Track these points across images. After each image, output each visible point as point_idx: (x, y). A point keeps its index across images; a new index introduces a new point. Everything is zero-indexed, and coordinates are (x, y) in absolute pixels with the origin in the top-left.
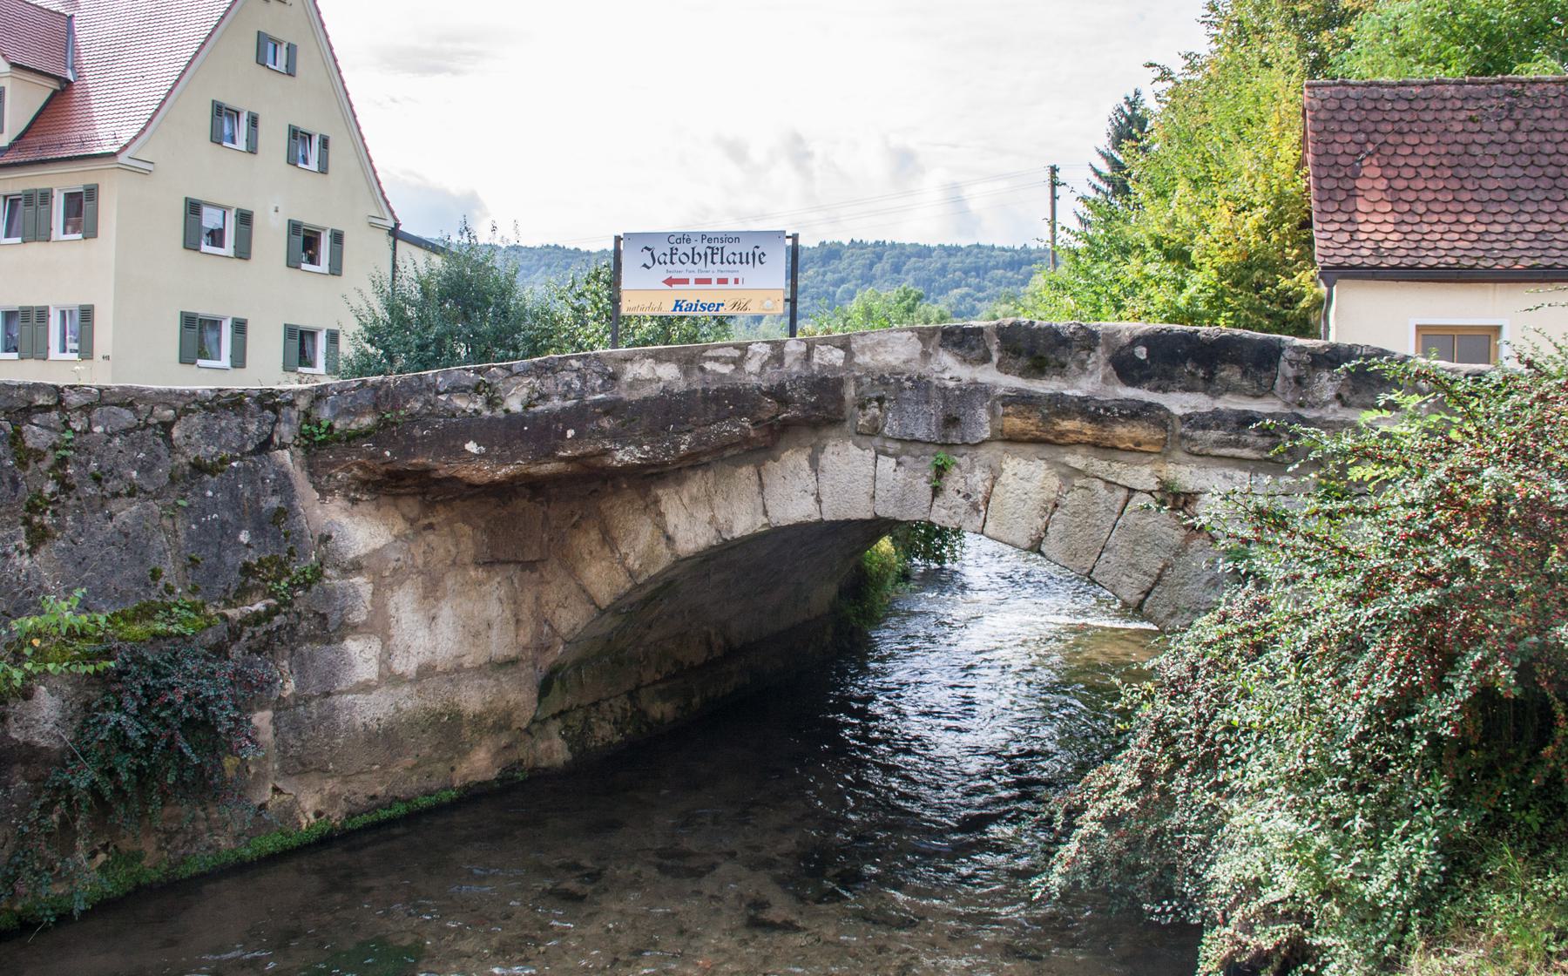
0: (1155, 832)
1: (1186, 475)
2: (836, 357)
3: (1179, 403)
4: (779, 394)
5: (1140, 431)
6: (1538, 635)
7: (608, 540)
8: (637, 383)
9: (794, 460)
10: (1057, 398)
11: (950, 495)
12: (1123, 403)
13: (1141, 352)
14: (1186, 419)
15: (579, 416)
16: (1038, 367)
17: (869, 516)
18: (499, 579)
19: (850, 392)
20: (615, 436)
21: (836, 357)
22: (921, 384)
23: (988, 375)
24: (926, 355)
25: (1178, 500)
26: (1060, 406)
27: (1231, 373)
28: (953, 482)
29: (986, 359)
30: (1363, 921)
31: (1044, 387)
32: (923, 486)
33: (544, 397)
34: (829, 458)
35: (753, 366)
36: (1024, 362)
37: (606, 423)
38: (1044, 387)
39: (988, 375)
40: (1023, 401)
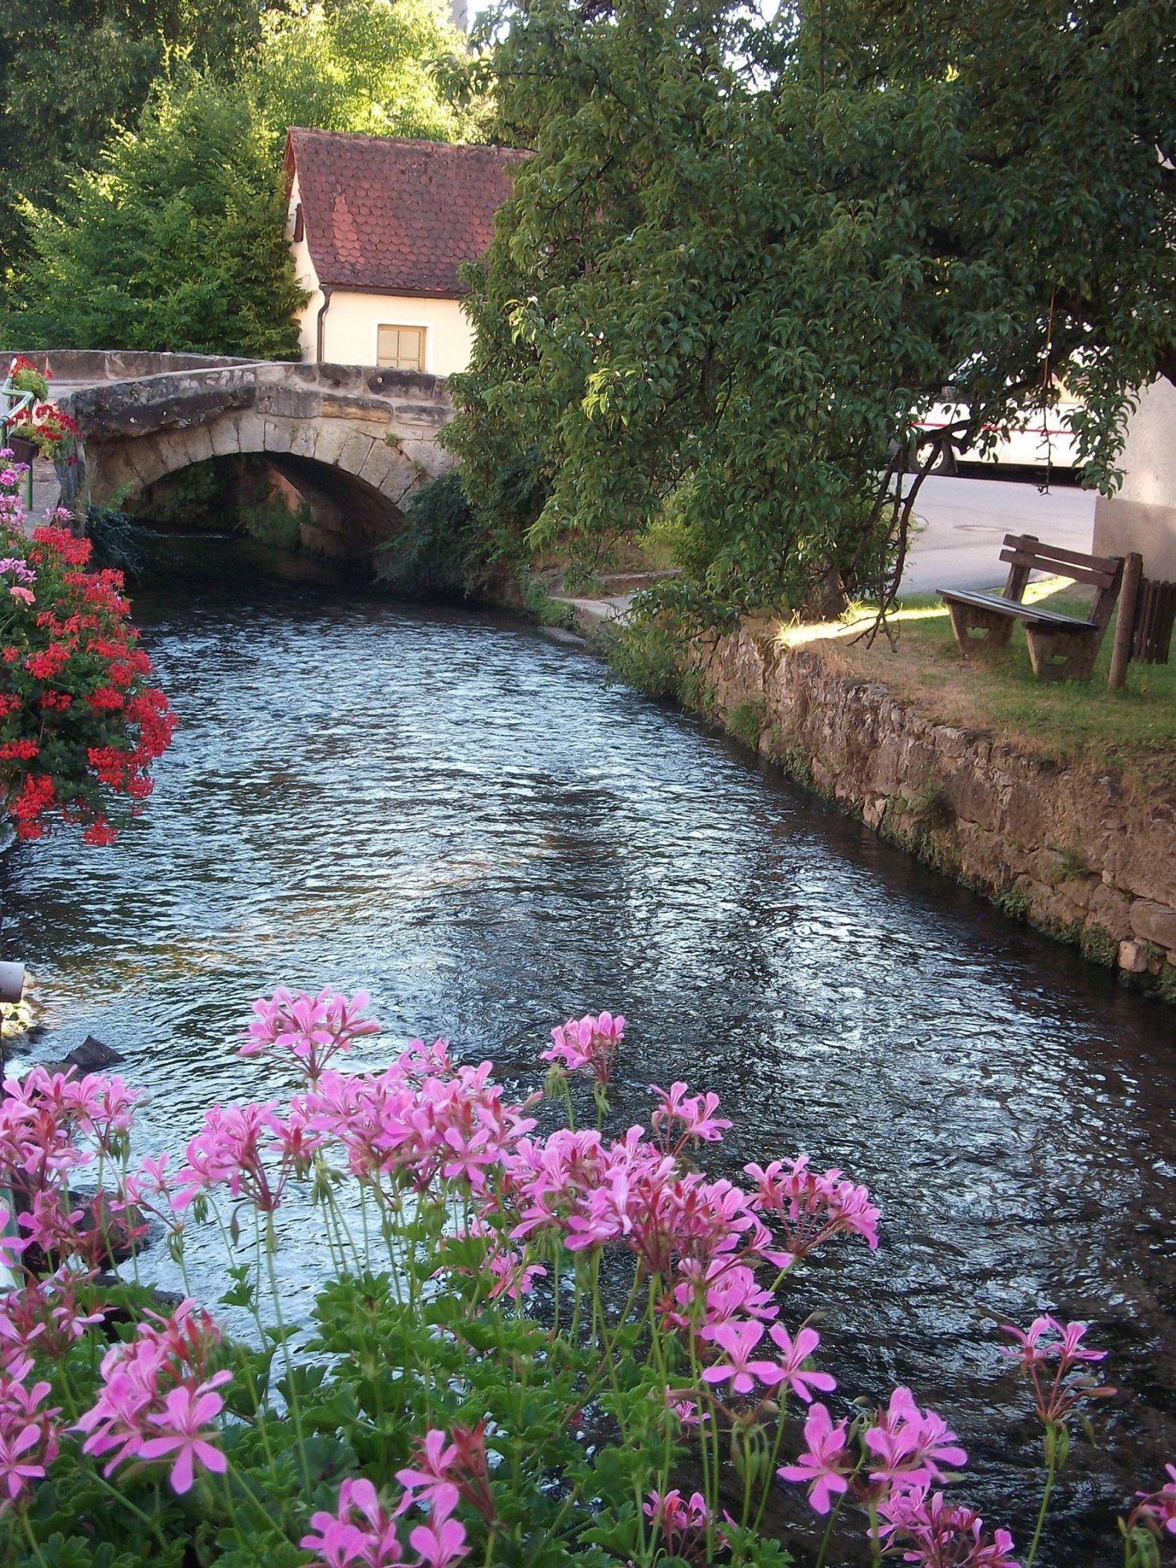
0: (430, 546)
1: (397, 430)
2: (251, 377)
3: (395, 402)
4: (234, 395)
5: (380, 414)
6: (1008, 1440)
7: (128, 463)
8: (185, 389)
9: (227, 424)
10: (345, 399)
11: (299, 441)
12: (373, 401)
13: (380, 380)
14: (399, 409)
15: (166, 405)
16: (337, 384)
17: (329, 459)
18: (436, 463)
19: (257, 393)
20: (179, 415)
21: (251, 377)
22: (288, 392)
23: (314, 387)
24: (287, 377)
25: (394, 442)
26: (347, 402)
27: (415, 390)
28: (301, 435)
29: (314, 379)
30: (619, 54)
31: (340, 393)
32: (287, 436)
33: (153, 397)
34: (244, 424)
35: (223, 382)
36: (330, 382)
37: (176, 409)
38: (340, 393)
39: (314, 387)
40: (330, 399)
